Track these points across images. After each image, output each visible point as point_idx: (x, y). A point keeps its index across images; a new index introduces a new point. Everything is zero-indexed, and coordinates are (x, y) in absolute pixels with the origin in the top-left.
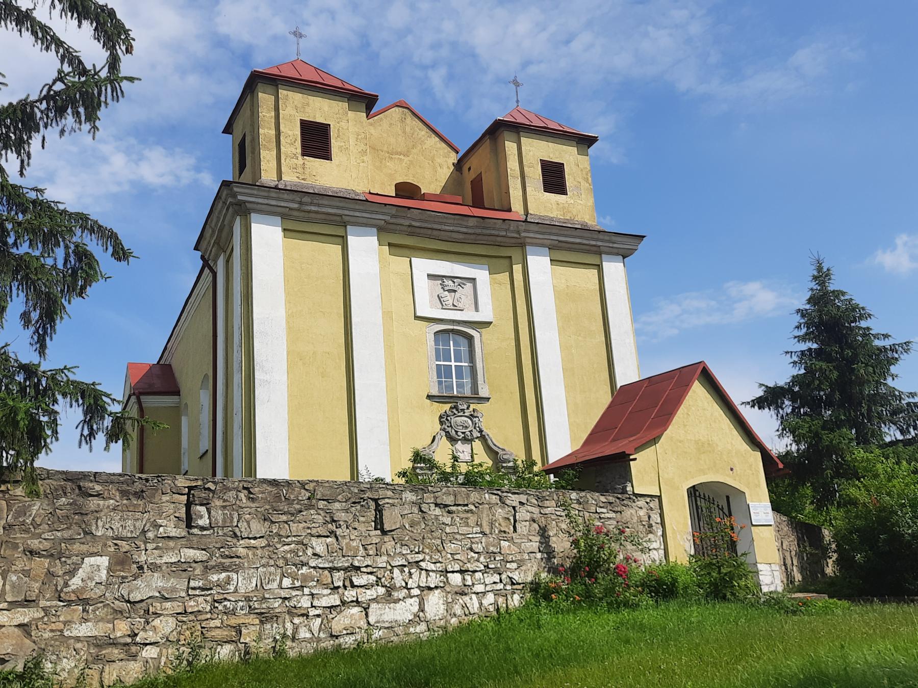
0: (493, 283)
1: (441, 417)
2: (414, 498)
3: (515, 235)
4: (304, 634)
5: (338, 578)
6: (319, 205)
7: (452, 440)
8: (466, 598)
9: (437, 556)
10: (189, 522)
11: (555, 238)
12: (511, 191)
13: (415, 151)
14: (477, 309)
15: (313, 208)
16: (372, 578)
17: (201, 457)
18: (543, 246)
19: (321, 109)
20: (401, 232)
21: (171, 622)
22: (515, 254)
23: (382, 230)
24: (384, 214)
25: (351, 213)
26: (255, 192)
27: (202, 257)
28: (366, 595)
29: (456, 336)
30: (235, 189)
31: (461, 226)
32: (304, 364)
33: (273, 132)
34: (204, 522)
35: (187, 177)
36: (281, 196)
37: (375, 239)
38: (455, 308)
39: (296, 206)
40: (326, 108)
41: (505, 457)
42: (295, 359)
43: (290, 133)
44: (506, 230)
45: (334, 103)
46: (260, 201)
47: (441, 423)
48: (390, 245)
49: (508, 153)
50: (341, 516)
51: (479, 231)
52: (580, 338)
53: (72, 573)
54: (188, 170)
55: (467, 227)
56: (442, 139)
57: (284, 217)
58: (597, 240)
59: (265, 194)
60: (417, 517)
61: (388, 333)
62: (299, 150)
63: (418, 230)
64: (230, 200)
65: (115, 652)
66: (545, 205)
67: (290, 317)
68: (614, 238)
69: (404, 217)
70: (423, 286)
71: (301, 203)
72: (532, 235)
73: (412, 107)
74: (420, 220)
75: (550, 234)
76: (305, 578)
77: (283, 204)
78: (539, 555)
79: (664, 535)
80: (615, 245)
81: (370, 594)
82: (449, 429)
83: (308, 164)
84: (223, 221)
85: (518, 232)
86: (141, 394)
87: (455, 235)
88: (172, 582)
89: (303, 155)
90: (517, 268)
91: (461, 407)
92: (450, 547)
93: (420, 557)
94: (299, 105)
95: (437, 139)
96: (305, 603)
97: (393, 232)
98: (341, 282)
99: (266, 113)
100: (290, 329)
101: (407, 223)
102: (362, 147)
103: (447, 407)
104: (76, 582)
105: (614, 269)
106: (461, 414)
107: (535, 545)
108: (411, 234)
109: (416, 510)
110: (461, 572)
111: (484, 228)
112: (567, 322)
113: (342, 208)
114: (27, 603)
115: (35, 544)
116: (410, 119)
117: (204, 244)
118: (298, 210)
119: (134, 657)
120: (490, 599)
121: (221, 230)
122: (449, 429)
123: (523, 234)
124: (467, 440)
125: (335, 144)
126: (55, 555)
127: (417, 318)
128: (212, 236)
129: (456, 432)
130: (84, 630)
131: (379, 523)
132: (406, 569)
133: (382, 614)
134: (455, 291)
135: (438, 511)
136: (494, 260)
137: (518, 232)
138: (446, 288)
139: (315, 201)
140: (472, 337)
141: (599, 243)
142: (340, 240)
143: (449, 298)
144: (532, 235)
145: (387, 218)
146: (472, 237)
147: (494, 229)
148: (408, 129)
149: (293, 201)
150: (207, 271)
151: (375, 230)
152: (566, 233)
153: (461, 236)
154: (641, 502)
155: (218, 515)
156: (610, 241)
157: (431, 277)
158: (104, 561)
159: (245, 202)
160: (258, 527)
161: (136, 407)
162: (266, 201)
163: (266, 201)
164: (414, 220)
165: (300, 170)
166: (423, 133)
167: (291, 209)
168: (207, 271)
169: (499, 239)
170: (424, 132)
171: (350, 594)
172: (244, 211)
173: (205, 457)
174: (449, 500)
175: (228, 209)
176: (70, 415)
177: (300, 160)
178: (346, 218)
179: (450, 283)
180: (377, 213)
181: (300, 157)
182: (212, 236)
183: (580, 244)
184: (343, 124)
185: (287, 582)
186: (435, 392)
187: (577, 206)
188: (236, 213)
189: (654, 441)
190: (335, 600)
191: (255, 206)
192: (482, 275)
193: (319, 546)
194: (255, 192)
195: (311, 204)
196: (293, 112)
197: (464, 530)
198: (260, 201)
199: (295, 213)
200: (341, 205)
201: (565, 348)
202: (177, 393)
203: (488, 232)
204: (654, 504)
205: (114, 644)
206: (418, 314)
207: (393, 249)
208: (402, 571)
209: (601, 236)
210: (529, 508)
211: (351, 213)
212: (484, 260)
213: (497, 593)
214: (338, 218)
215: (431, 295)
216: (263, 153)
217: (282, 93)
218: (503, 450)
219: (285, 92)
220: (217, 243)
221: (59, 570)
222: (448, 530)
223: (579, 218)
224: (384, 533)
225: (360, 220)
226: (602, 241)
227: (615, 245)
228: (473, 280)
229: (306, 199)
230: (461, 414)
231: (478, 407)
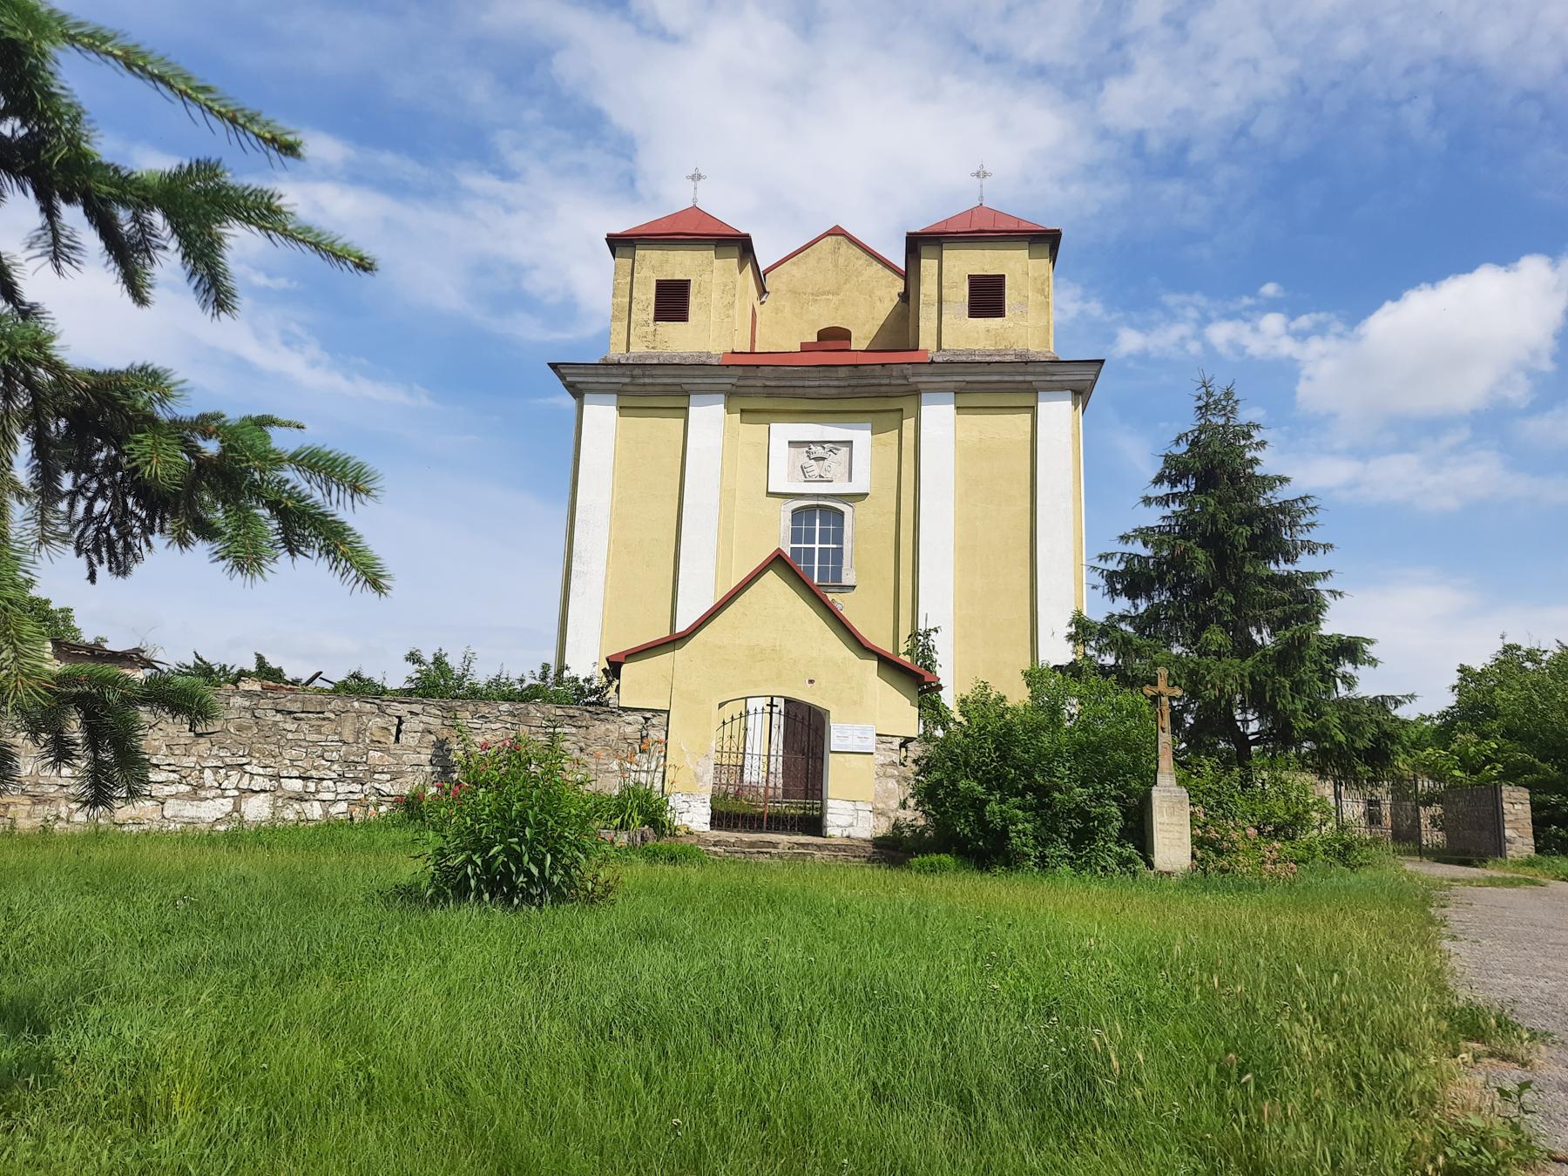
2: (247, 704)
6: (652, 376)
8: (306, 805)
14: (850, 479)
15: (647, 381)
16: (174, 776)
20: (756, 395)
23: (732, 395)
24: (730, 376)
31: (830, 379)
35: (1073, 309)
38: (822, 479)
39: (627, 380)
51: (853, 382)
54: (1075, 301)
57: (619, 393)
62: (652, 316)
68: (1051, 369)
69: (755, 377)
70: (781, 454)
71: (632, 377)
75: (952, 374)
78: (428, 769)
81: (167, 790)
85: (905, 377)
90: (909, 424)
93: (244, 760)
97: (743, 395)
101: (759, 383)
105: (1057, 413)
107: (425, 756)
108: (770, 396)
109: (248, 715)
111: (861, 377)
112: (969, 486)
113: (680, 376)
123: (912, 380)
127: (769, 494)
132: (223, 771)
133: (190, 810)
135: (279, 717)
143: (815, 469)
145: (734, 381)
147: (874, 377)
148: (841, 260)
149: (623, 375)
153: (833, 391)
156: (1046, 374)
164: (768, 379)
165: (650, 337)
169: (883, 389)
174: (296, 707)
178: (686, 387)
180: (720, 376)
184: (706, 277)
192: (861, 436)
195: (644, 376)
197: (314, 737)
199: (630, 388)
207: (747, 417)
208: (215, 773)
209: (1030, 368)
210: (425, 719)
212: (868, 416)
213: (351, 803)
222: (290, 736)
225: (702, 387)
226: (1033, 374)
229: (637, 372)
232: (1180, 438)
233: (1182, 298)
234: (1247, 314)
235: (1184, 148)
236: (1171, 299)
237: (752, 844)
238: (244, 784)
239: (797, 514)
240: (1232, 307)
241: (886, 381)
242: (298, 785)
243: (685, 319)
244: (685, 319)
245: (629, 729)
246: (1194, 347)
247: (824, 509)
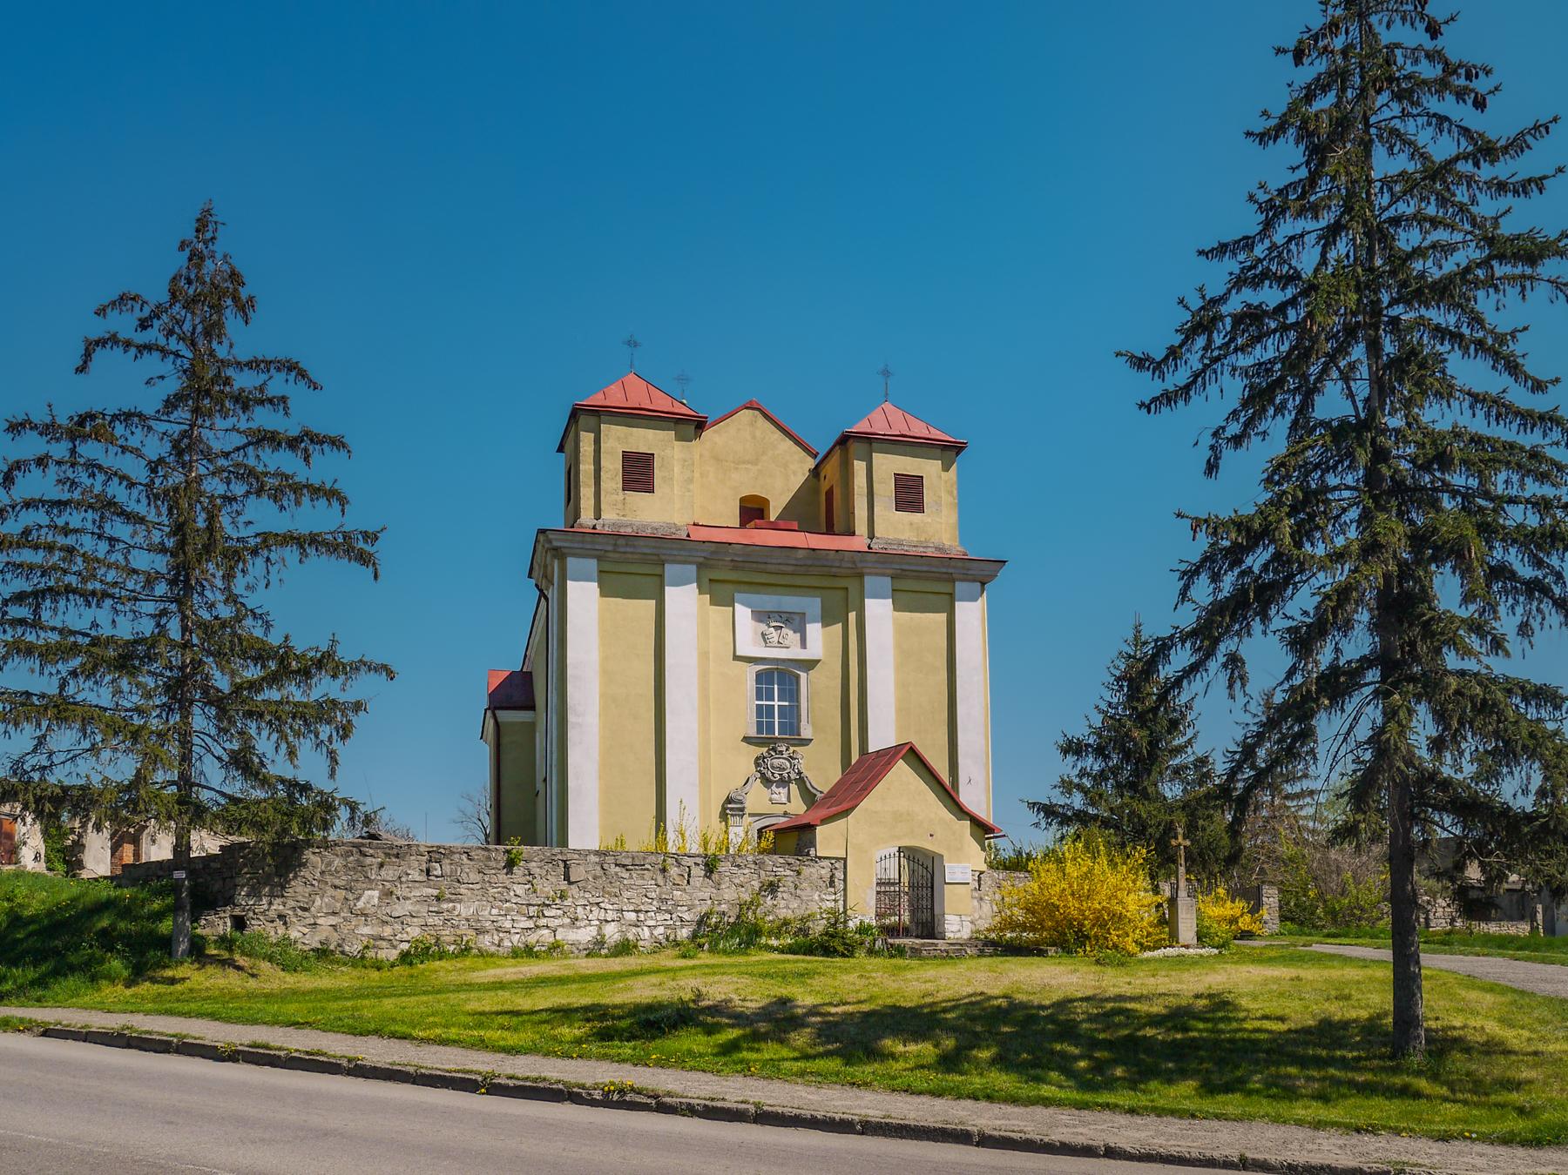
4: (507, 943)
5: (533, 911)
7: (767, 782)
9: (615, 900)
10: (428, 872)
18: (883, 575)
19: (643, 439)
21: (418, 930)
22: (852, 584)
28: (553, 923)
29: (779, 678)
34: (438, 872)
47: (757, 765)
50: (537, 871)
53: (358, 899)
56: (798, 442)
57: (599, 559)
60: (599, 871)
61: (704, 676)
65: (384, 944)
66: (896, 528)
73: (765, 407)
76: (508, 909)
79: (845, 890)
81: (557, 922)
86: (496, 708)
88: (418, 907)
92: (626, 894)
96: (508, 925)
104: (360, 904)
108: (735, 568)
110: (637, 912)
112: (905, 656)
114: (334, 913)
115: (337, 882)
116: (761, 420)
117: (535, 574)
119: (395, 947)
120: (661, 930)
124: (784, 782)
126: (349, 889)
127: (736, 658)
130: (366, 930)
131: (567, 878)
148: (758, 434)
154: (826, 863)
155: (447, 869)
158: (376, 893)
160: (474, 877)
165: (620, 506)
170: (778, 435)
171: (543, 922)
176: (344, 813)
185: (495, 911)
186: (753, 732)
187: (937, 527)
189: (845, 813)
190: (530, 924)
193: (520, 890)
197: (641, 882)
201: (902, 685)
204: (839, 865)
205: (382, 939)
221: (350, 896)
223: (936, 540)
224: (570, 883)
232: (123, 300)
238: (602, 915)
239: (759, 676)
242: (633, 916)
243: (650, 489)
244: (650, 489)
245: (823, 872)
247: (781, 673)
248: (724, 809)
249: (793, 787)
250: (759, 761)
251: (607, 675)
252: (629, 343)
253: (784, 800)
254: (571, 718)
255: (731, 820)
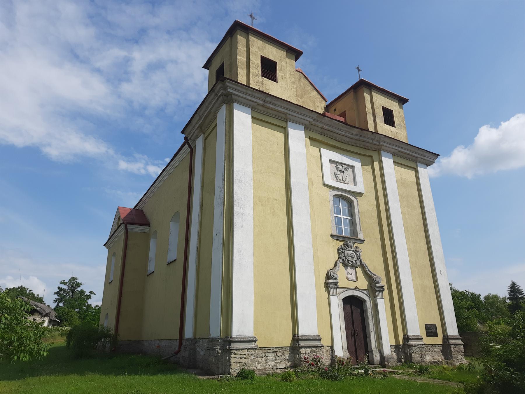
0: (363, 170)
1: (338, 250)
3: (377, 143)
6: (274, 104)
7: (345, 265)
11: (397, 148)
12: (368, 120)
13: (305, 96)
14: (355, 184)
17: (169, 264)
19: (273, 53)
22: (375, 155)
23: (307, 128)
24: (310, 117)
25: (292, 113)
26: (239, 88)
27: (186, 138)
29: (346, 199)
30: (227, 84)
32: (262, 205)
33: (245, 59)
36: (254, 94)
37: (303, 133)
38: (343, 182)
39: (261, 102)
40: (275, 53)
41: (377, 280)
42: (258, 201)
43: (255, 62)
44: (373, 139)
45: (279, 51)
46: (241, 95)
47: (339, 254)
48: (311, 139)
49: (366, 99)
51: (358, 137)
52: (409, 210)
55: (352, 134)
58: (417, 153)
59: (245, 91)
61: (310, 192)
62: (260, 73)
63: (326, 131)
64: (222, 91)
67: (255, 172)
69: (320, 122)
70: (327, 165)
71: (264, 101)
72: (385, 144)
74: (329, 125)
75: (395, 145)
77: (254, 100)
80: (425, 158)
82: (344, 258)
83: (265, 82)
84: (211, 109)
85: (379, 142)
87: (345, 138)
89: (262, 76)
90: (376, 164)
91: (350, 245)
94: (261, 47)
95: (316, 93)
98: (284, 155)
99: (241, 48)
100: (254, 180)
101: (321, 125)
102: (293, 79)
103: (341, 243)
106: (350, 249)
108: (321, 134)
111: (361, 136)
113: (288, 109)
116: (303, 79)
118: (263, 106)
121: (207, 116)
122: (344, 258)
123: (382, 143)
124: (354, 266)
125: (279, 74)
127: (325, 185)
128: (197, 123)
129: (348, 260)
134: (343, 172)
136: (363, 157)
137: (379, 142)
138: (339, 170)
139: (273, 102)
140: (352, 201)
141: (418, 156)
142: (283, 130)
143: (340, 175)
144: (385, 144)
145: (312, 120)
146: (354, 141)
147: (366, 138)
148: (302, 84)
149: (260, 99)
150: (186, 146)
151: (303, 127)
152: (403, 146)
153: (348, 139)
157: (331, 161)
159: (231, 94)
161: (124, 231)
162: (244, 96)
163: (244, 96)
164: (326, 125)
165: (260, 84)
166: (310, 88)
167: (258, 104)
168: (186, 146)
169: (368, 144)
170: (310, 88)
172: (229, 100)
173: (171, 265)
175: (218, 99)
177: (260, 79)
178: (289, 116)
179: (341, 167)
180: (306, 116)
181: (260, 77)
182: (197, 123)
183: (408, 154)
184: (284, 63)
186: (335, 233)
188: (224, 102)
191: (237, 98)
192: (357, 165)
194: (239, 88)
195: (271, 103)
196: (257, 50)
198: (241, 95)
199: (260, 108)
200: (287, 107)
202: (148, 225)
203: (363, 139)
206: (326, 182)
209: (419, 152)
211: (292, 113)
214: (284, 116)
215: (331, 173)
216: (239, 70)
217: (251, 38)
218: (375, 275)
219: (253, 38)
220: (200, 127)
226: (419, 154)
227: (425, 158)
228: (352, 167)
229: (268, 99)
230: (350, 249)
231: (358, 245)
233: (141, 156)
234: (160, 165)
235: (145, 108)
236: (137, 156)
237: (212, 378)
240: (156, 162)
241: (371, 141)
246: (143, 172)
248: (326, 284)
249: (359, 270)
250: (340, 251)
251: (257, 185)
252: (251, 16)
253: (354, 279)
254: (236, 209)
255: (332, 291)
